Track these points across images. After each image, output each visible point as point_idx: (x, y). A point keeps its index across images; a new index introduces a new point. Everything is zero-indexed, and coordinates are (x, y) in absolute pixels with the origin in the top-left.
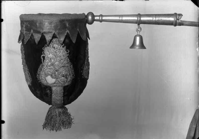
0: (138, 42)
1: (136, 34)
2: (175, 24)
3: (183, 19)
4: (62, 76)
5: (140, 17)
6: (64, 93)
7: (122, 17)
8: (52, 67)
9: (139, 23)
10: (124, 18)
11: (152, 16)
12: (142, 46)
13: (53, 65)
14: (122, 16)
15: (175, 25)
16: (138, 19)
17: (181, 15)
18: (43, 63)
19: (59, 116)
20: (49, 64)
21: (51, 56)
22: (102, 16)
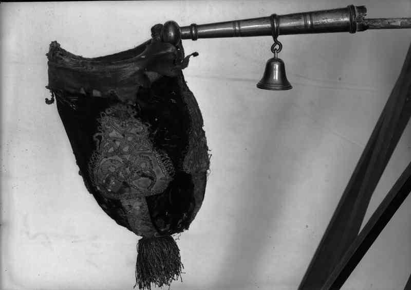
0: (276, 76)
1: (271, 56)
2: (349, 28)
3: (369, 15)
4: (140, 174)
5: (278, 22)
6: (151, 212)
7: (306, 25)
8: (116, 157)
9: (274, 33)
10: (244, 27)
11: (303, 18)
12: (285, 84)
13: (126, 164)
14: (239, 22)
15: (353, 31)
16: (273, 25)
17: (362, 9)
18: (98, 149)
19: (101, 132)
20: (112, 150)
21: (113, 134)
22: (194, 26)
